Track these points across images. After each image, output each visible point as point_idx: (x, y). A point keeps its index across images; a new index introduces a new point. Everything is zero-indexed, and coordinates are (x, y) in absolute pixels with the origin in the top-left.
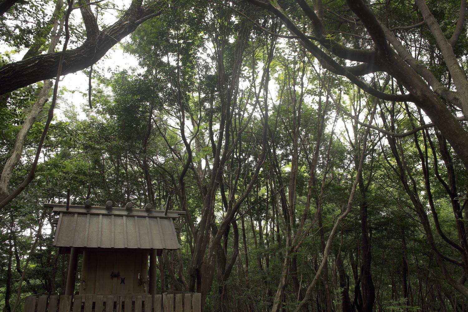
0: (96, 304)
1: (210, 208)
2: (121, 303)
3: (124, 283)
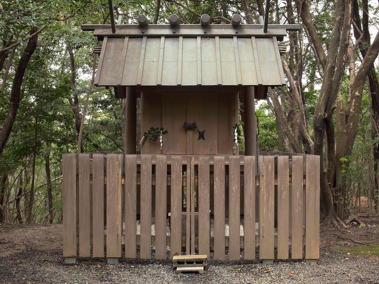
0: (157, 167)
1: (345, 17)
2: (193, 167)
3: (203, 138)
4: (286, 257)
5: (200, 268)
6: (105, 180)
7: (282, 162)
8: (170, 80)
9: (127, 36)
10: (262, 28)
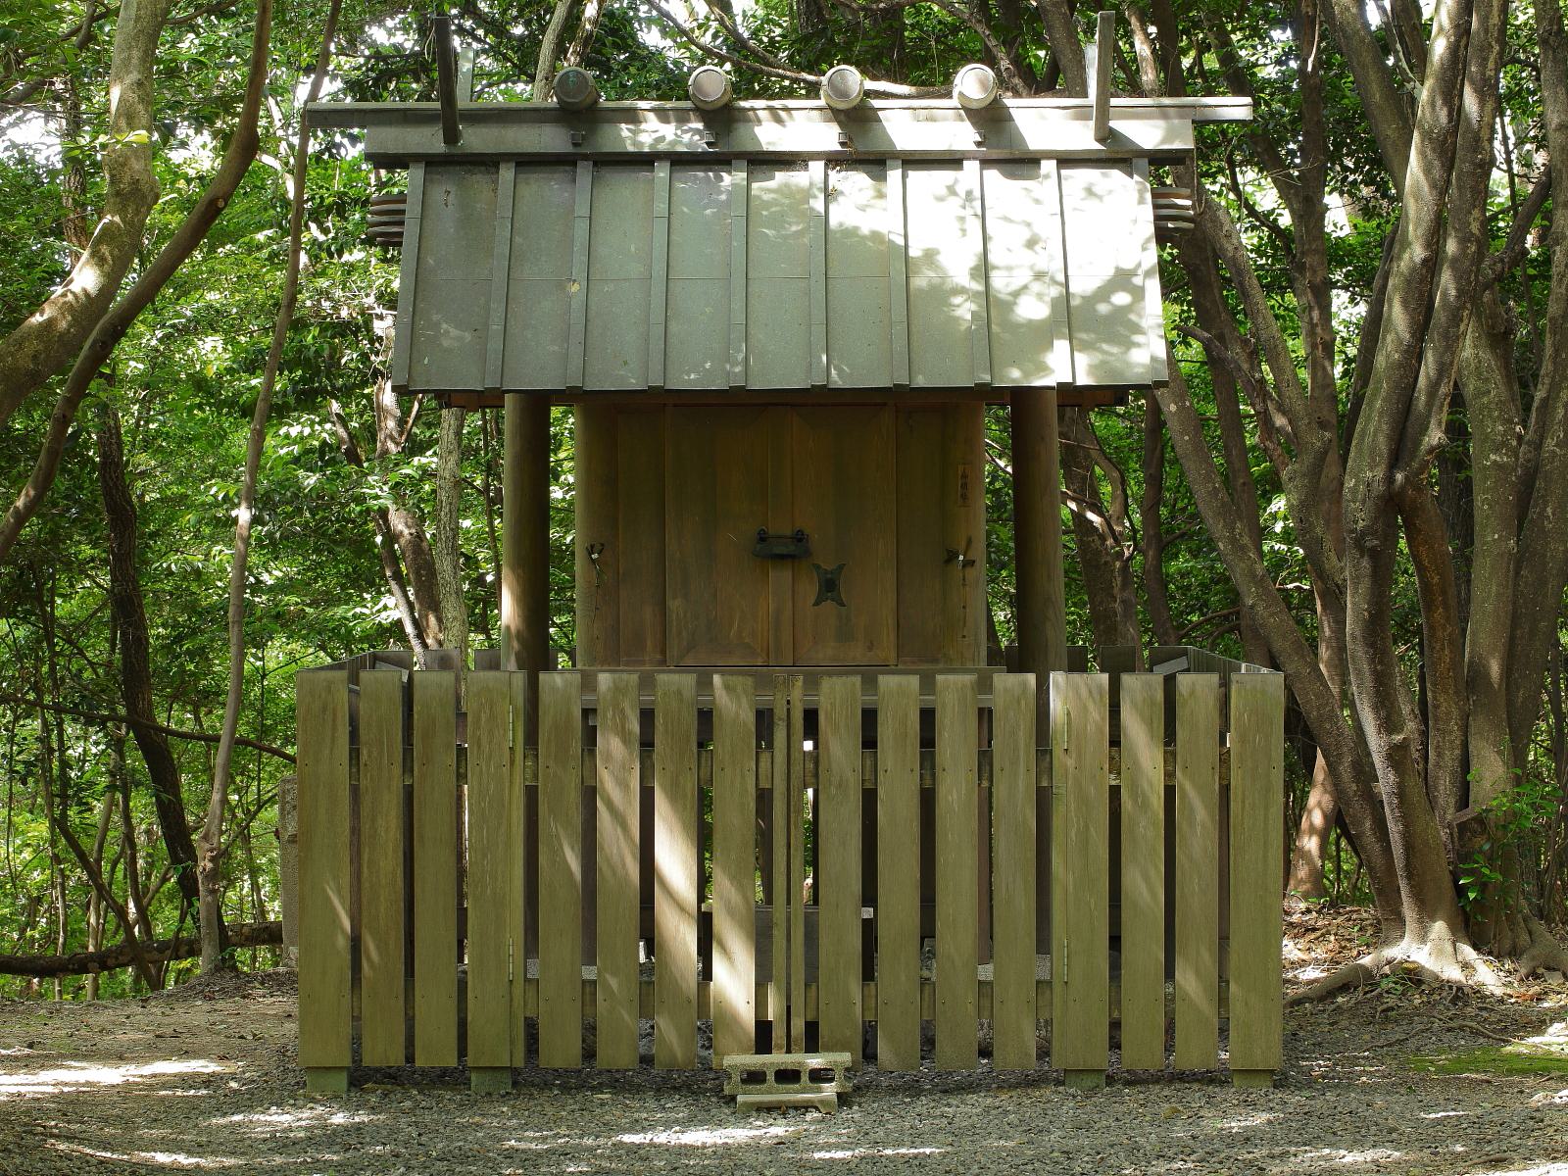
6: (462, 771)
9: (508, 161)
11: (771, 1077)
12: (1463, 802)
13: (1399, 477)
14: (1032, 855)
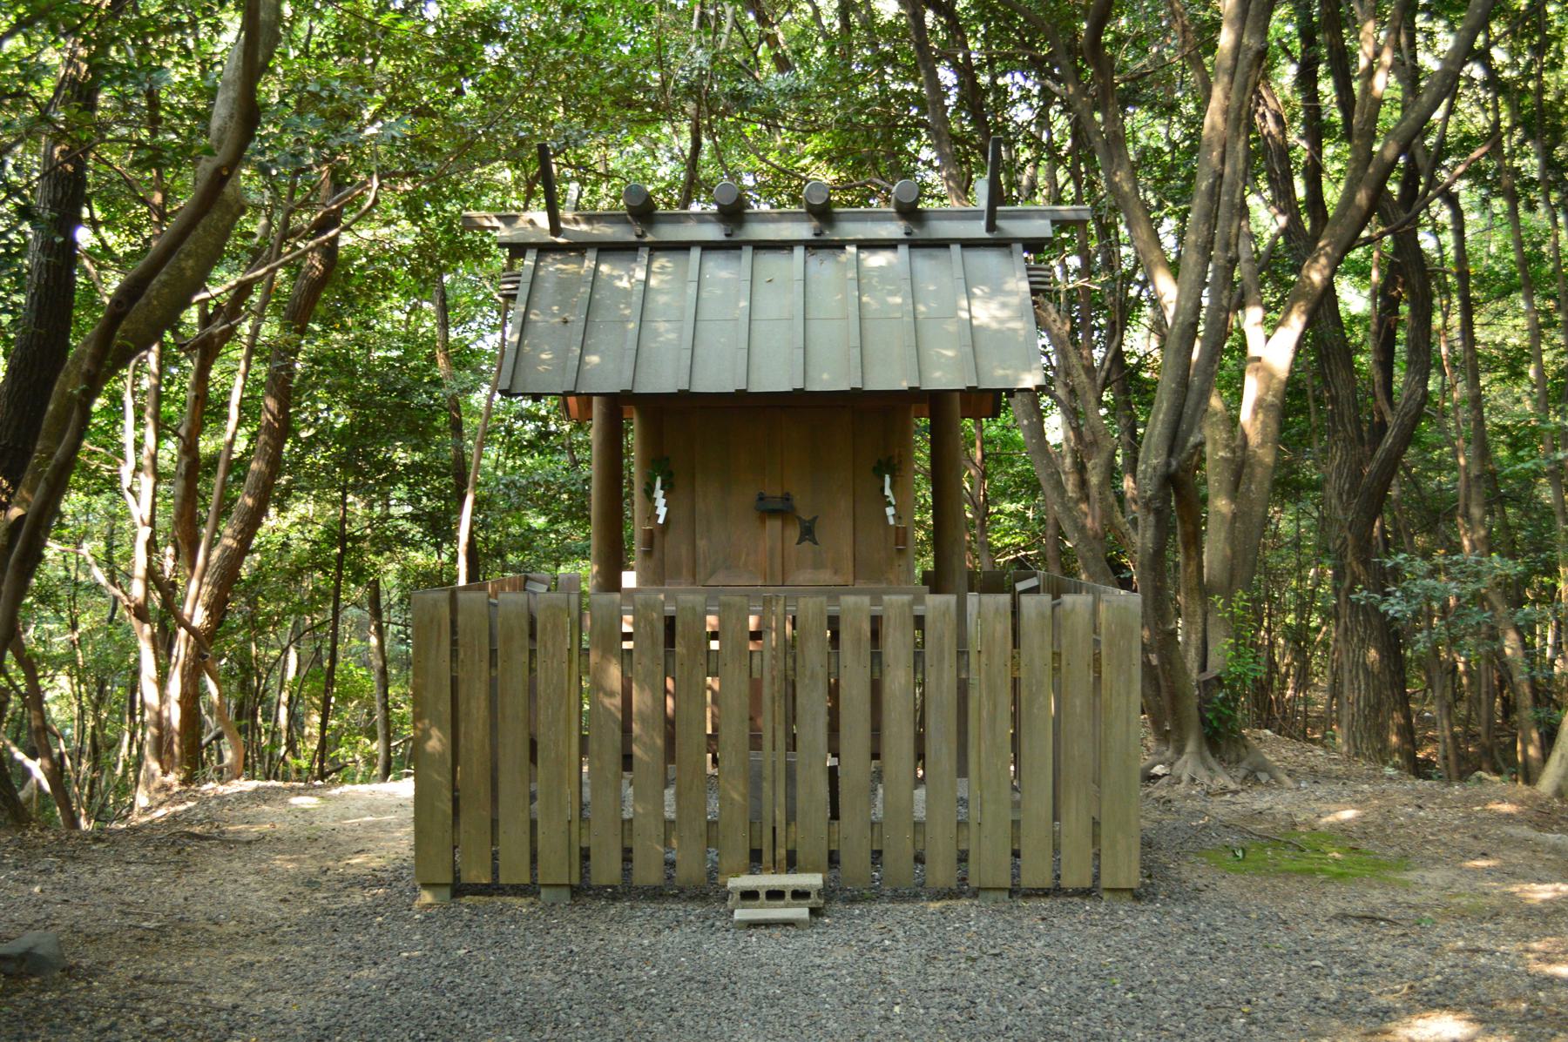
4: (1046, 881)
5: (800, 912)
7: (1033, 615)
8: (718, 376)
10: (980, 218)
11: (762, 896)
12: (1203, 667)
13: (1174, 463)
14: (953, 728)
